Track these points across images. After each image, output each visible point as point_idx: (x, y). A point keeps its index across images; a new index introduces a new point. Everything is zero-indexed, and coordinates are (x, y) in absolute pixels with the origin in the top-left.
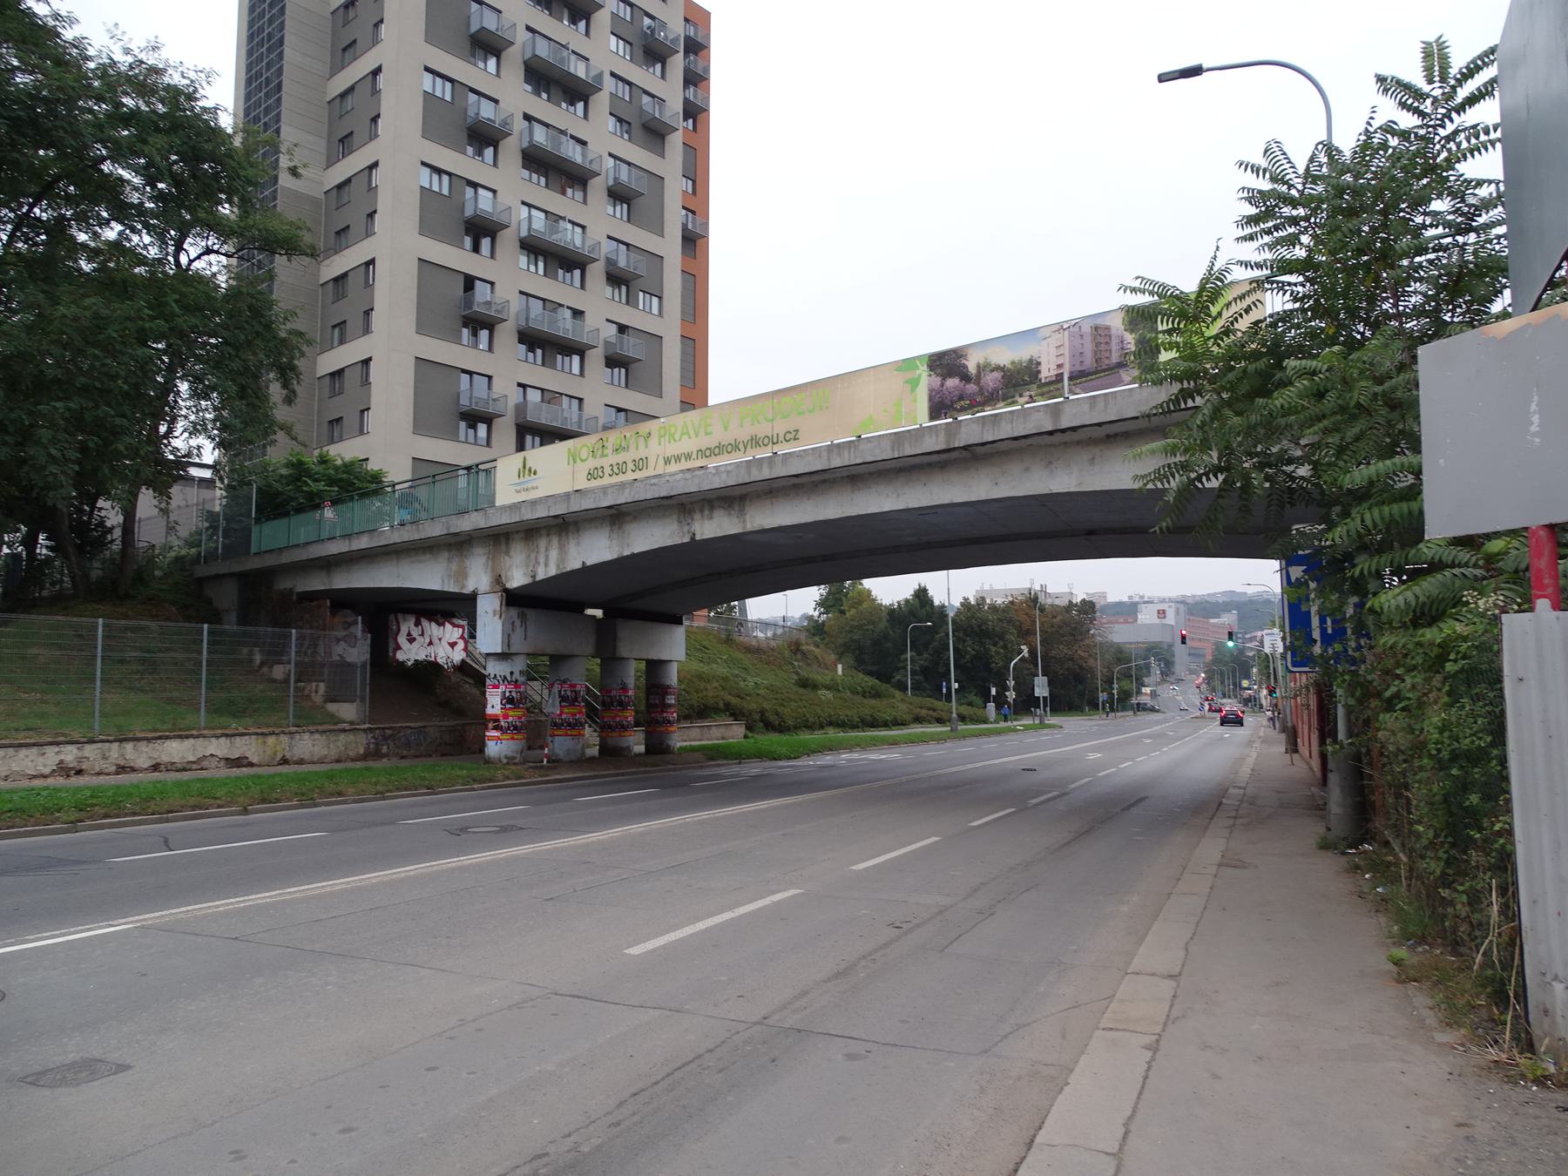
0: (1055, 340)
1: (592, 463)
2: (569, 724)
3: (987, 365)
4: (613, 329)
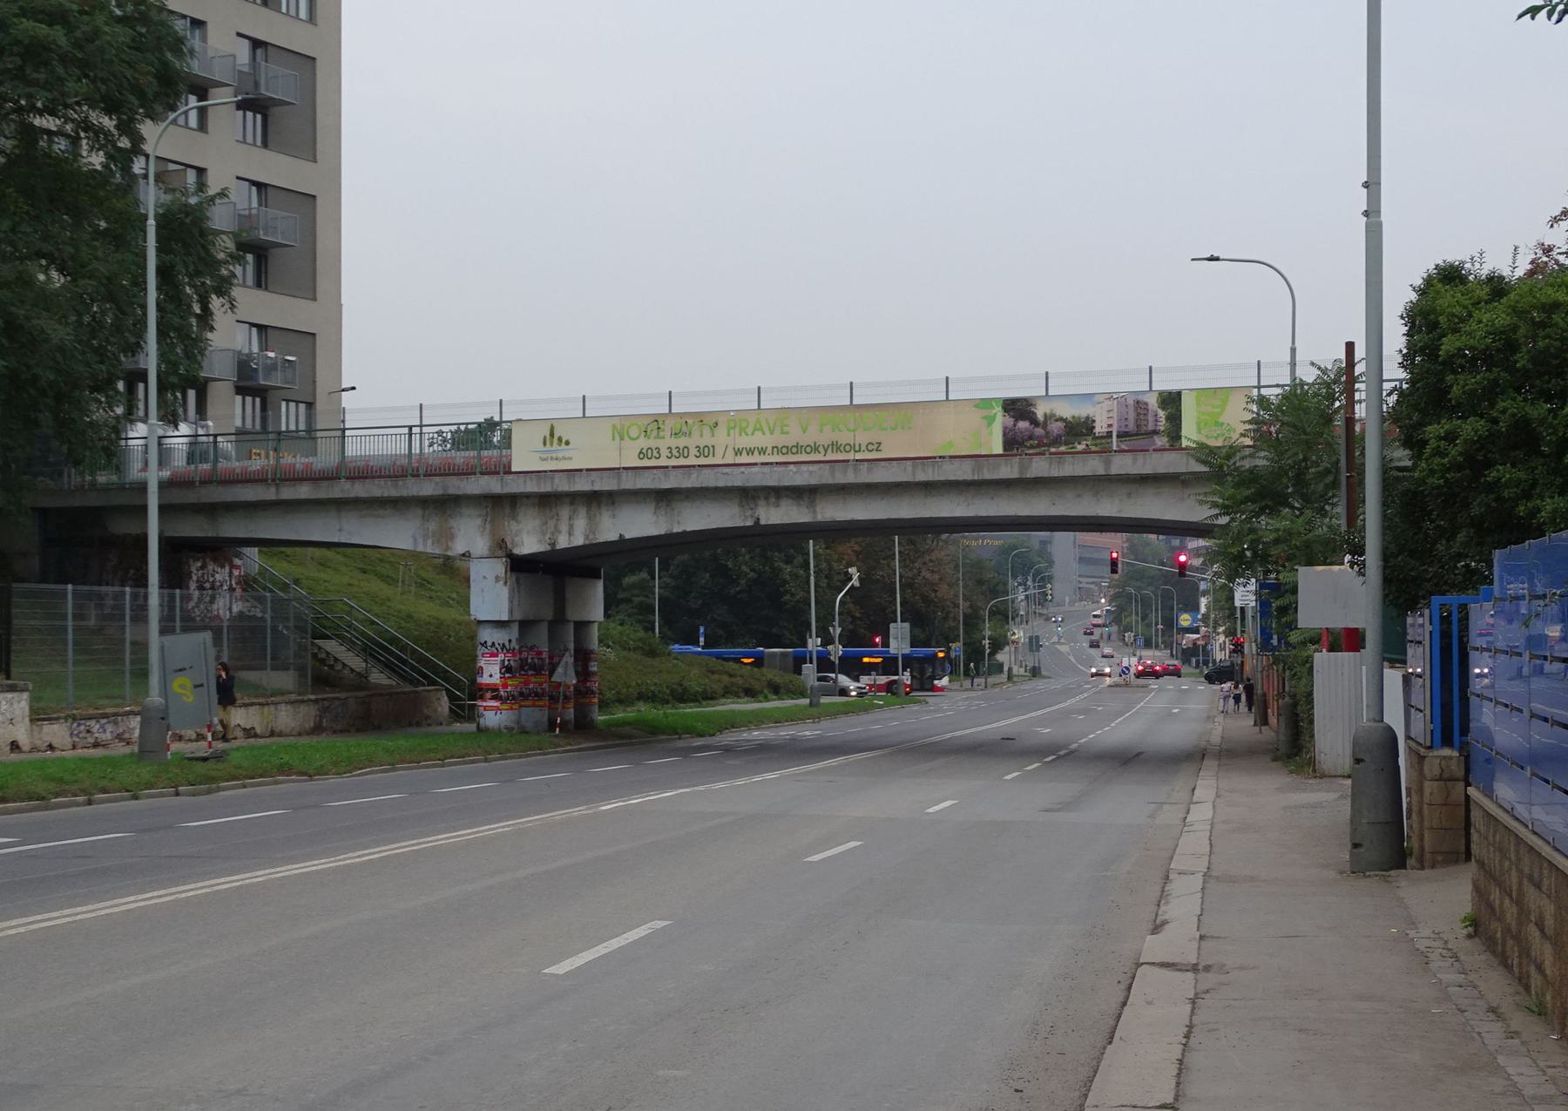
0: (1107, 405)
1: (643, 443)
2: (537, 694)
3: (1052, 415)
4: (244, 48)
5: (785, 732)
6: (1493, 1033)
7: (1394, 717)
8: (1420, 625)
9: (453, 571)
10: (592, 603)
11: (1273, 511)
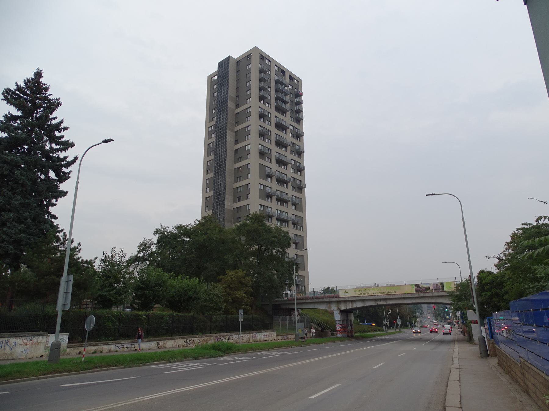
1: (359, 292)
5: (383, 337)
6: (500, 375)
7: (484, 334)
8: (486, 321)
9: (332, 314)
10: (352, 317)
11: (461, 301)
